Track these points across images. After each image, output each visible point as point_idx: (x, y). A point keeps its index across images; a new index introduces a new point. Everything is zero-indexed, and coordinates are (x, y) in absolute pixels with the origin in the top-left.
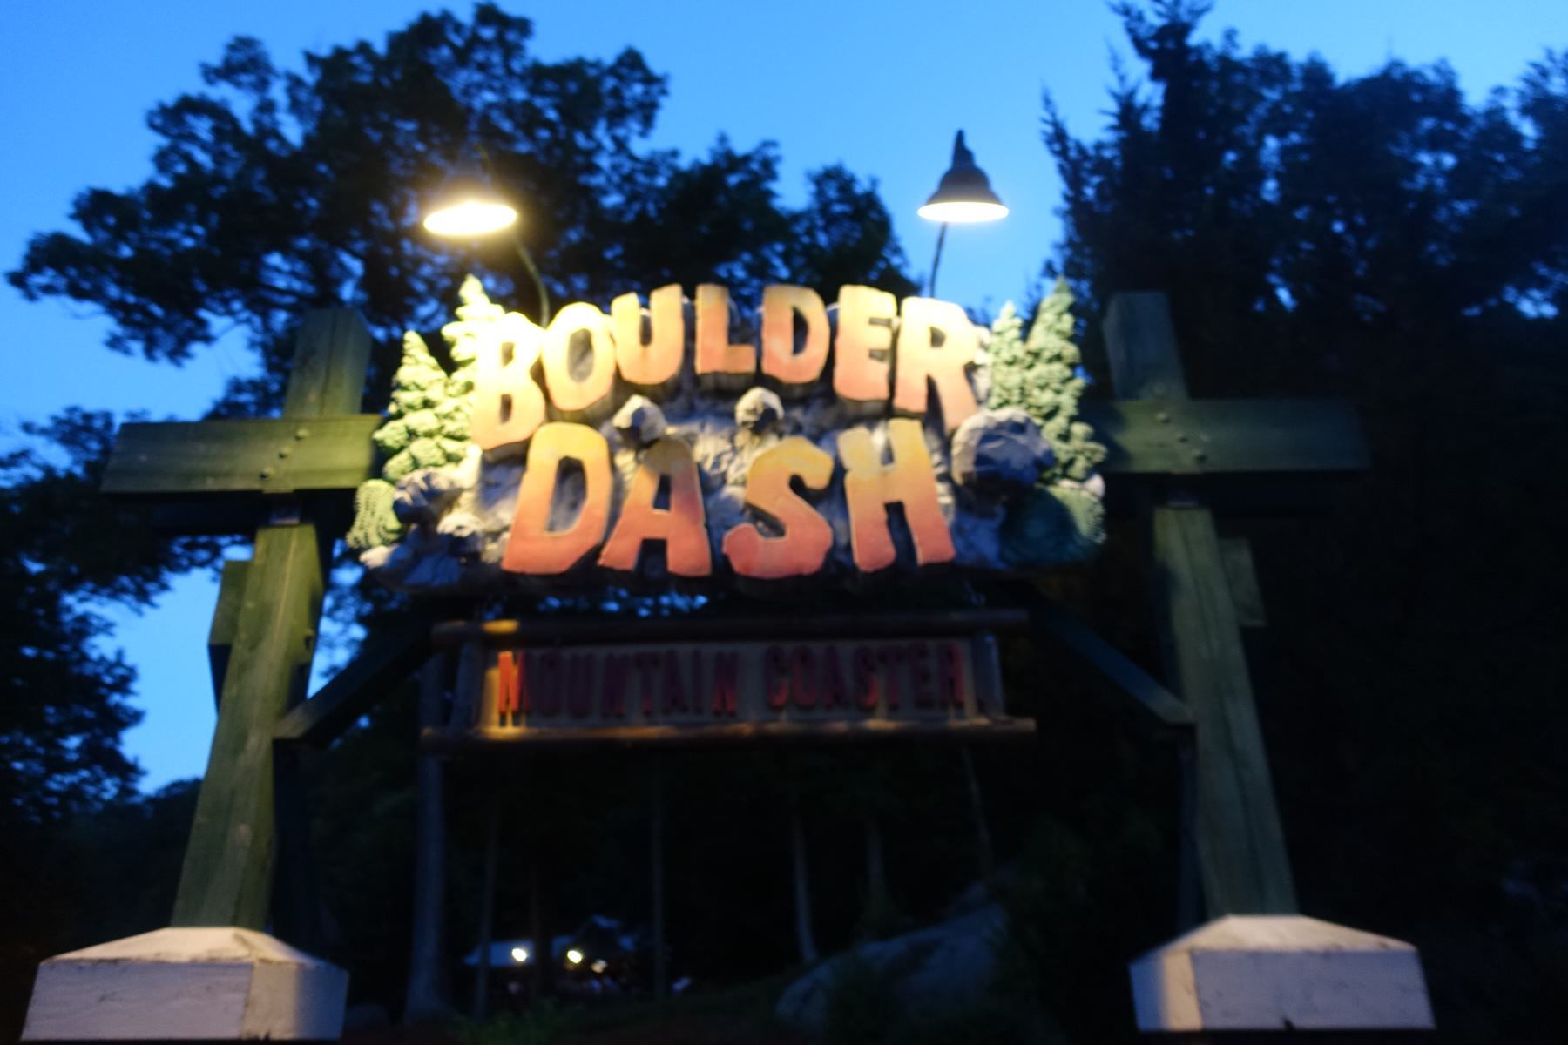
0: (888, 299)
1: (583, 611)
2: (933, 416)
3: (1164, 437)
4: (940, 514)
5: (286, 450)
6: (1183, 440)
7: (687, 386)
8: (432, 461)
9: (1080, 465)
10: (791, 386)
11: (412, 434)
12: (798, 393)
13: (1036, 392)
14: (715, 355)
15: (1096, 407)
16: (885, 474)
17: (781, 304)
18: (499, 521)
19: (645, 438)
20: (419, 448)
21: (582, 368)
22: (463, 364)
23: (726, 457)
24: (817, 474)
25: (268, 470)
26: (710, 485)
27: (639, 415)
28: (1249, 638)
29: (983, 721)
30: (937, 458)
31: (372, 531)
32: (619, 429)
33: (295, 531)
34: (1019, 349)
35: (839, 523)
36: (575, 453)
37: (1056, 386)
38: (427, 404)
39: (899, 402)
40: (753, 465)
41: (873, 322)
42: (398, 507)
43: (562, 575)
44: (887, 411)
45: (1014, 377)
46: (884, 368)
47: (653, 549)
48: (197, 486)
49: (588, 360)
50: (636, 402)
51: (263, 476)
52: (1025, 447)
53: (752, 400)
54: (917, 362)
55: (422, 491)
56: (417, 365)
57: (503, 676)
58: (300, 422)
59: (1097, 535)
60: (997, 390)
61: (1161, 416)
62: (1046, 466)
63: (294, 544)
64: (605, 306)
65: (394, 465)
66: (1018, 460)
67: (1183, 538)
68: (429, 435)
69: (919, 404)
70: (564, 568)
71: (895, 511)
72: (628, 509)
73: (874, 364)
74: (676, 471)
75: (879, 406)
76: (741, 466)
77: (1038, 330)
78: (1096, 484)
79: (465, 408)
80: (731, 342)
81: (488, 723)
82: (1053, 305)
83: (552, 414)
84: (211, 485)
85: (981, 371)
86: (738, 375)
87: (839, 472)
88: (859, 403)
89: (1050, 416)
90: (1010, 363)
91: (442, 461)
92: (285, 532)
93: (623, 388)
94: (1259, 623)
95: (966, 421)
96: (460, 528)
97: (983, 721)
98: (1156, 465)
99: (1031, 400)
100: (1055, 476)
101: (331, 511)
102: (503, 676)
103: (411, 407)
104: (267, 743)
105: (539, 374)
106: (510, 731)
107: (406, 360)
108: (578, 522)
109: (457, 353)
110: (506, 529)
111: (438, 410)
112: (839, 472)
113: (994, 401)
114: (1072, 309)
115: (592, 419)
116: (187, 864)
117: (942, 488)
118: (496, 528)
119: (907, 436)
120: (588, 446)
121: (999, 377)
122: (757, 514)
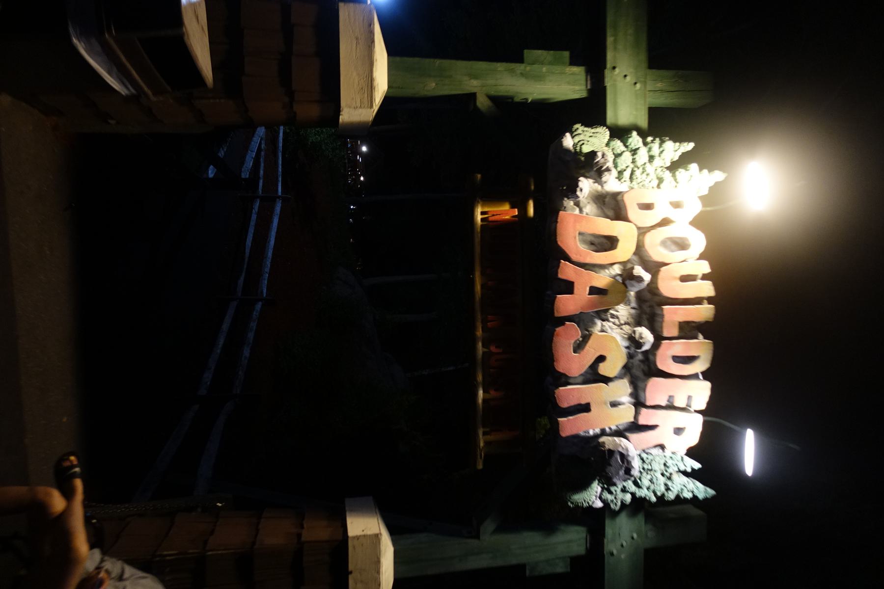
0: (703, 406)
1: (535, 257)
2: (636, 427)
3: (624, 538)
4: (584, 429)
5: (628, 78)
6: (622, 546)
7: (657, 299)
8: (619, 164)
9: (609, 497)
10: (655, 355)
11: (634, 152)
12: (651, 357)
13: (649, 477)
14: (673, 316)
15: (638, 505)
16: (605, 403)
17: (702, 350)
18: (585, 207)
19: (627, 282)
20: (627, 157)
21: (669, 243)
22: (674, 176)
23: (616, 321)
24: (604, 369)
25: (617, 70)
26: (602, 314)
27: (640, 279)
28: (522, 567)
29: (482, 444)
30: (614, 428)
31: (581, 137)
32: (633, 268)
33: (584, 87)
34: (673, 469)
35: (580, 380)
36: (620, 245)
37: (652, 487)
38: (651, 158)
39: (644, 411)
40: (612, 338)
41: (689, 398)
42: (593, 154)
43: (556, 242)
44: (639, 404)
45: (658, 467)
46: (663, 403)
47: (568, 287)
48: (609, 32)
49: (673, 247)
50: (647, 277)
51: (614, 68)
52: (618, 474)
53: (647, 336)
54: (666, 421)
55: (602, 167)
56: (672, 150)
57: (505, 211)
58: (644, 83)
59: (572, 503)
60: (650, 457)
61: (635, 536)
62: (608, 483)
63: (577, 88)
64: (702, 257)
65: (618, 145)
66: (611, 470)
67: (572, 540)
68: (634, 161)
69: (642, 421)
70: (559, 243)
71: (585, 408)
72: (588, 274)
73: (666, 398)
74: (608, 298)
75: (642, 400)
76: (611, 329)
77: (685, 479)
78: (599, 504)
79: (649, 178)
80: (680, 323)
81: (483, 206)
82: (697, 488)
83: (643, 232)
84: (610, 40)
85: (661, 451)
86: (662, 327)
87: (606, 380)
88: (644, 390)
89: (636, 483)
90: (665, 465)
91: (619, 169)
92: (584, 82)
93: (654, 268)
94: (566, 54)
95: (632, 446)
96: (581, 190)
97: (482, 444)
98: (609, 531)
99: (644, 474)
100: (603, 484)
101: (592, 110)
102: (505, 211)
103: (650, 150)
104: (473, 90)
105: (665, 222)
106: (479, 217)
107: (678, 144)
108: (582, 247)
109: (681, 173)
110: (581, 211)
111: (648, 165)
112: (606, 380)
113: (644, 456)
114: (695, 497)
115: (639, 250)
116: (417, 59)
117: (598, 431)
118: (581, 205)
119: (625, 415)
120: (625, 251)
121: (657, 459)
122: (586, 338)
